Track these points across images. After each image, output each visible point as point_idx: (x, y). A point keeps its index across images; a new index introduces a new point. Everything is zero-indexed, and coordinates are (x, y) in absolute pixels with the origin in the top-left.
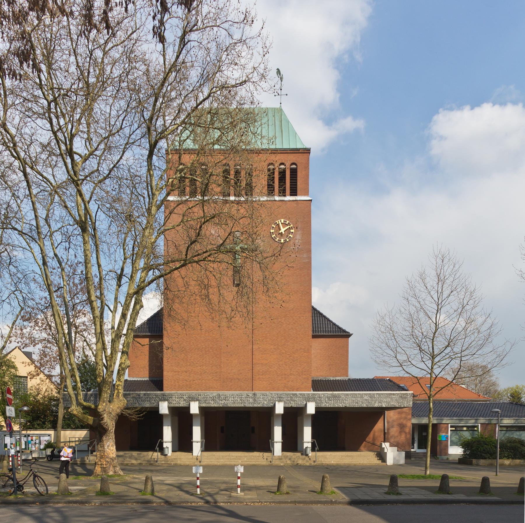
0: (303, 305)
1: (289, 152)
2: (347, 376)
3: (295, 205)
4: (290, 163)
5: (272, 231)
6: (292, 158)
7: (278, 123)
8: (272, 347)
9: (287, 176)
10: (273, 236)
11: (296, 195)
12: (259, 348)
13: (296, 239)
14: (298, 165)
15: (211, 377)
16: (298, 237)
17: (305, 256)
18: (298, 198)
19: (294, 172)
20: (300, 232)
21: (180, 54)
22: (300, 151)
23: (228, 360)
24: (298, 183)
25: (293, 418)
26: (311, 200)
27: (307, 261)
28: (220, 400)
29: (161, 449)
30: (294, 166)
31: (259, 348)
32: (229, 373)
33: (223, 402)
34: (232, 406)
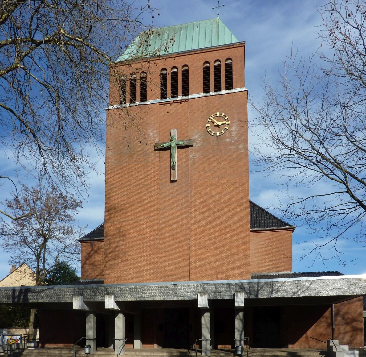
0: (240, 196)
1: (224, 48)
2: (291, 271)
3: (231, 98)
4: (225, 59)
5: (207, 125)
6: (227, 53)
7: (214, 30)
8: (209, 241)
9: (225, 76)
10: (208, 131)
11: (232, 89)
12: (196, 243)
13: (232, 131)
14: (233, 59)
15: (148, 275)
16: (234, 128)
17: (242, 146)
18: (234, 91)
19: (229, 67)
20: (236, 123)
21: (273, 276)
22: (235, 46)
23: (165, 257)
24: (234, 77)
25: (222, 309)
26: (247, 90)
27: (244, 151)
28: (137, 293)
29: (232, 342)
30: (230, 61)
31: (196, 243)
32: (166, 270)
33: (140, 296)
34: (150, 300)
